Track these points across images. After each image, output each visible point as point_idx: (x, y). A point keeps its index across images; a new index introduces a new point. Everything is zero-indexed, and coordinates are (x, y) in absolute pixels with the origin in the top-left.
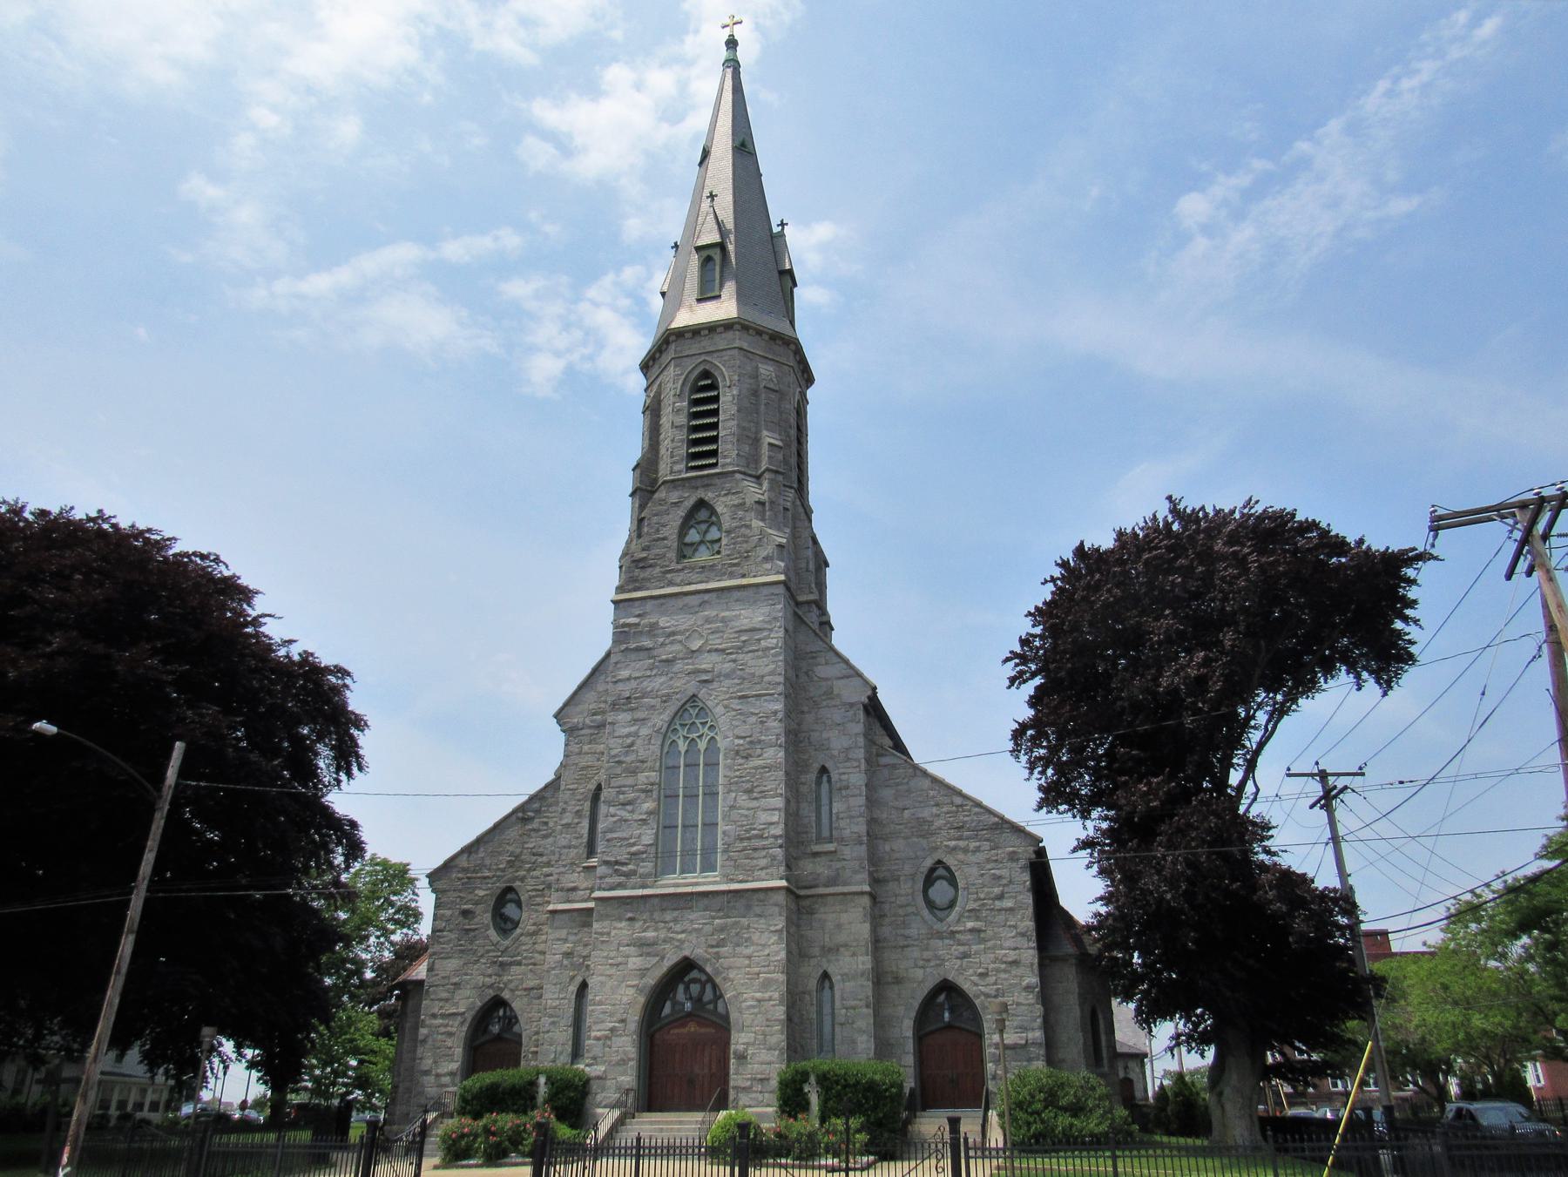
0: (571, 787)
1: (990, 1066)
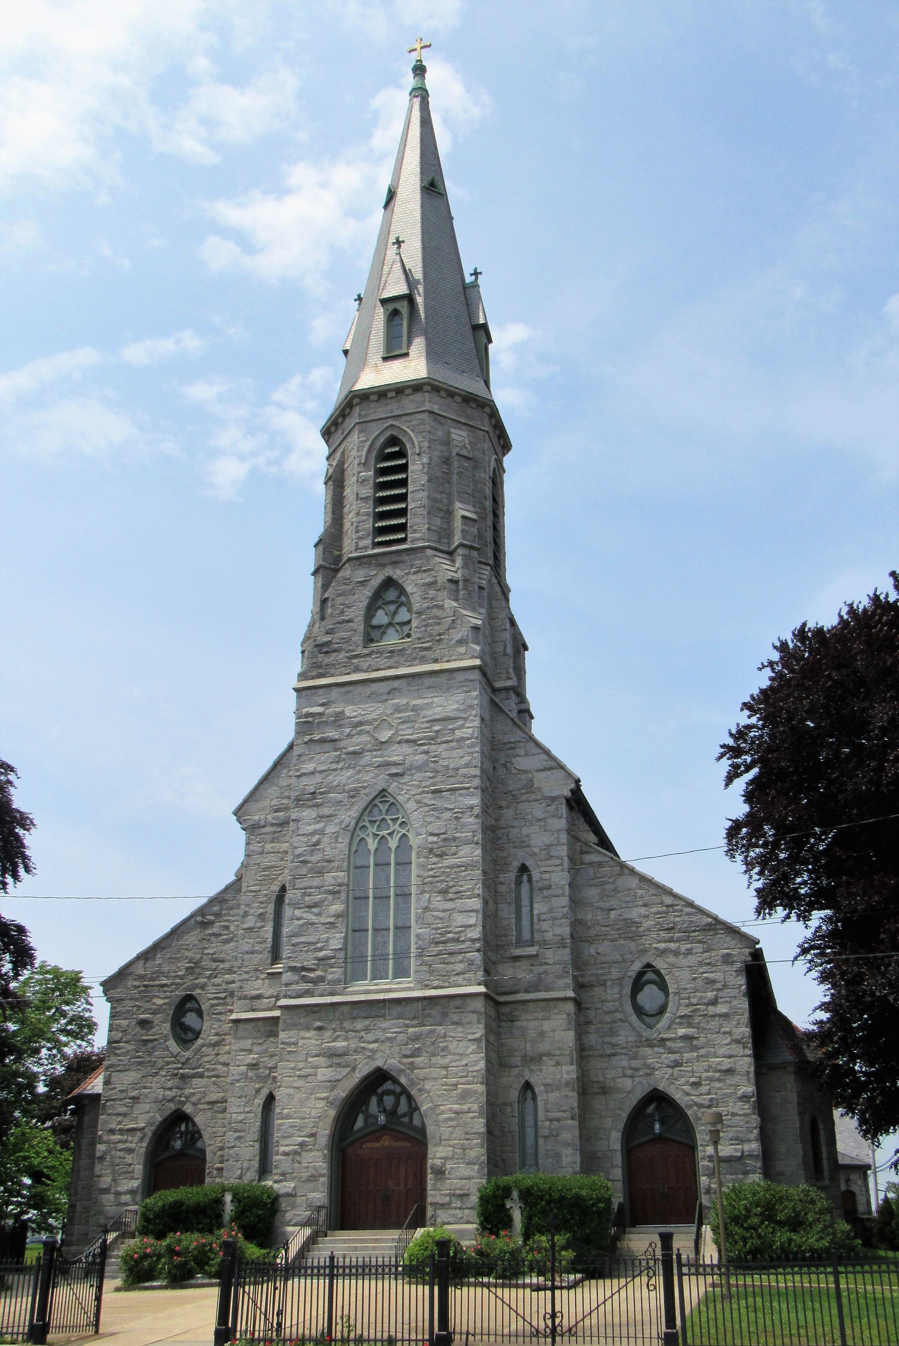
0: (254, 888)
1: (704, 1180)
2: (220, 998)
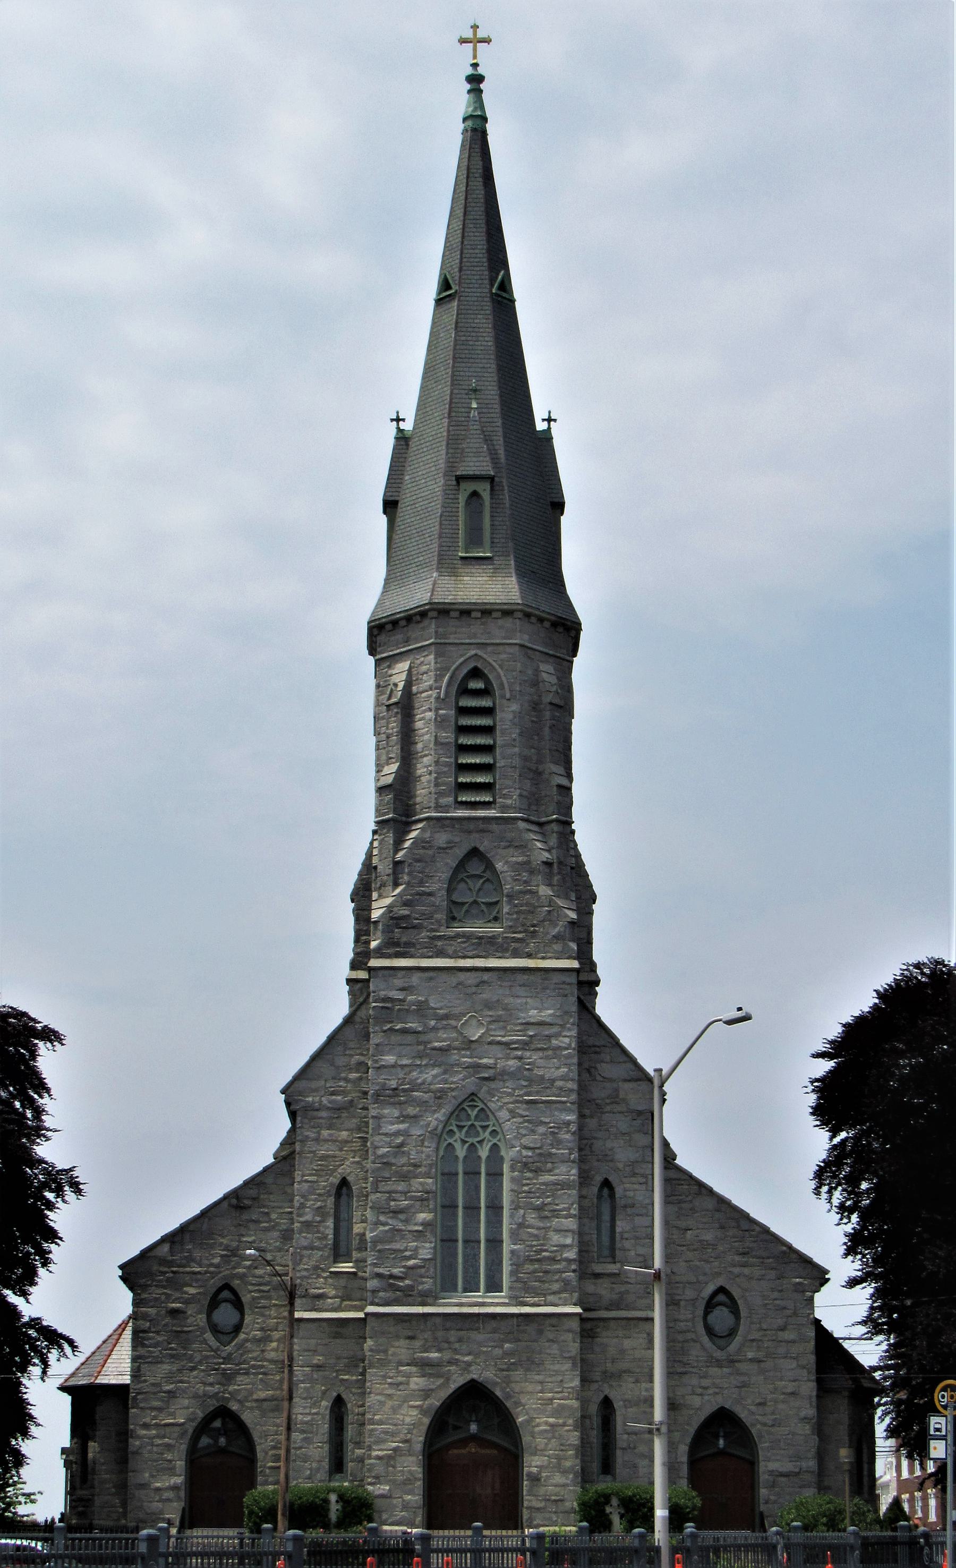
0: (310, 1178)
1: (763, 1492)
2: (264, 1291)
